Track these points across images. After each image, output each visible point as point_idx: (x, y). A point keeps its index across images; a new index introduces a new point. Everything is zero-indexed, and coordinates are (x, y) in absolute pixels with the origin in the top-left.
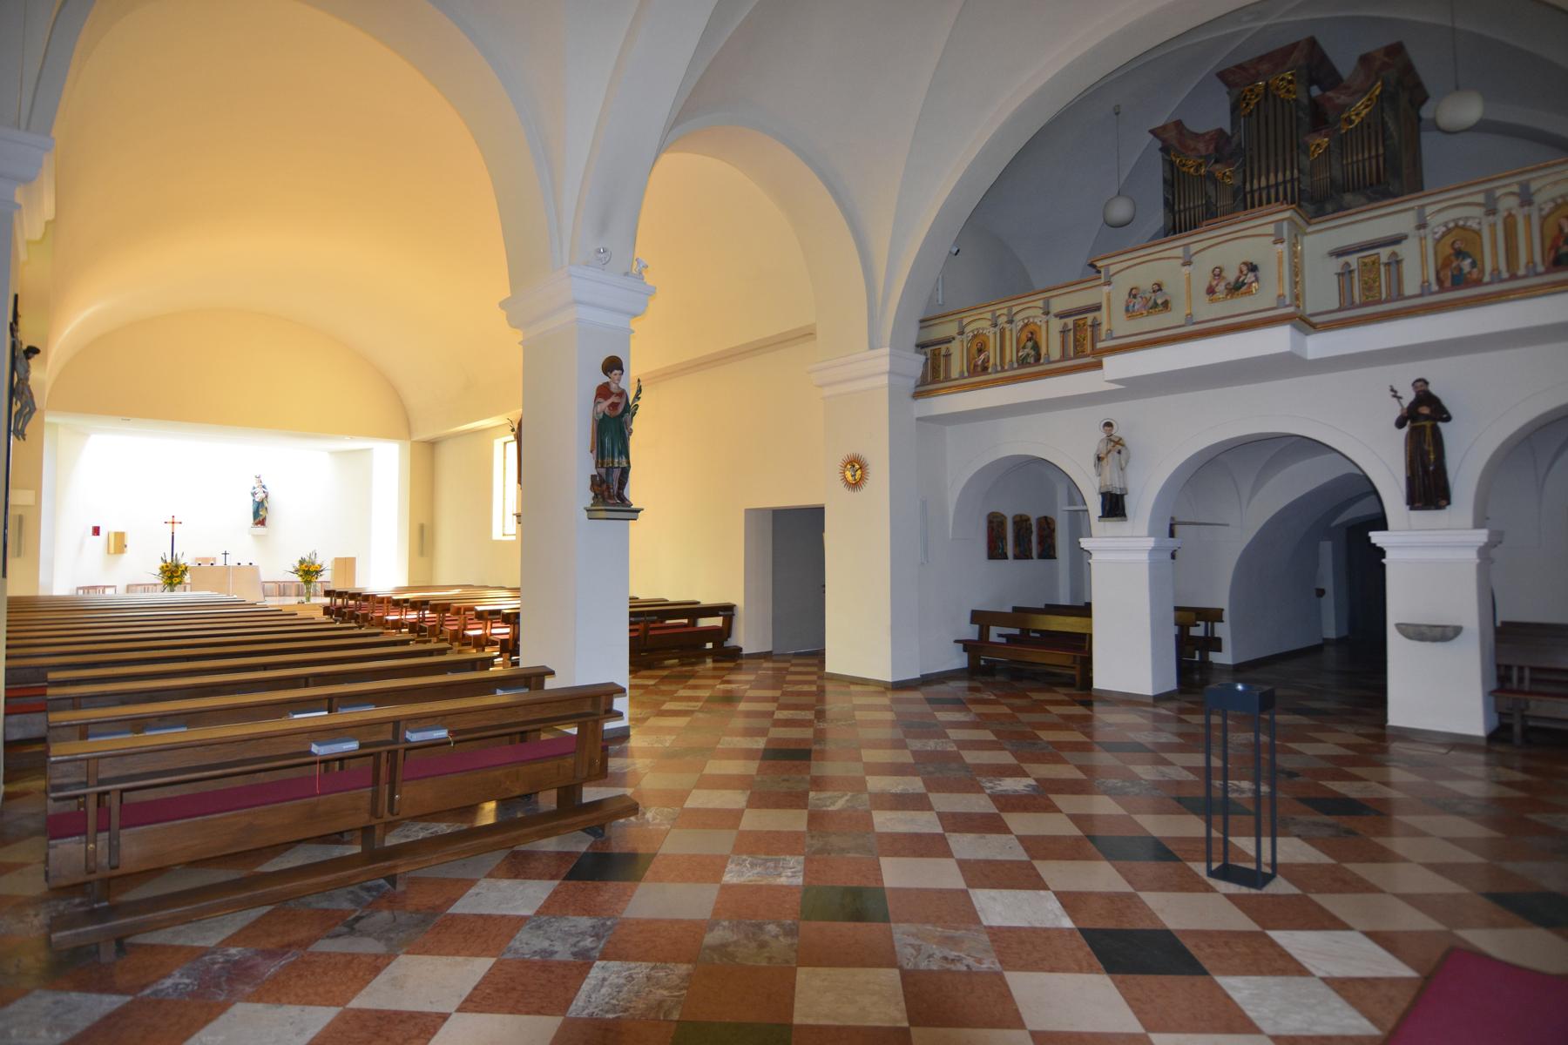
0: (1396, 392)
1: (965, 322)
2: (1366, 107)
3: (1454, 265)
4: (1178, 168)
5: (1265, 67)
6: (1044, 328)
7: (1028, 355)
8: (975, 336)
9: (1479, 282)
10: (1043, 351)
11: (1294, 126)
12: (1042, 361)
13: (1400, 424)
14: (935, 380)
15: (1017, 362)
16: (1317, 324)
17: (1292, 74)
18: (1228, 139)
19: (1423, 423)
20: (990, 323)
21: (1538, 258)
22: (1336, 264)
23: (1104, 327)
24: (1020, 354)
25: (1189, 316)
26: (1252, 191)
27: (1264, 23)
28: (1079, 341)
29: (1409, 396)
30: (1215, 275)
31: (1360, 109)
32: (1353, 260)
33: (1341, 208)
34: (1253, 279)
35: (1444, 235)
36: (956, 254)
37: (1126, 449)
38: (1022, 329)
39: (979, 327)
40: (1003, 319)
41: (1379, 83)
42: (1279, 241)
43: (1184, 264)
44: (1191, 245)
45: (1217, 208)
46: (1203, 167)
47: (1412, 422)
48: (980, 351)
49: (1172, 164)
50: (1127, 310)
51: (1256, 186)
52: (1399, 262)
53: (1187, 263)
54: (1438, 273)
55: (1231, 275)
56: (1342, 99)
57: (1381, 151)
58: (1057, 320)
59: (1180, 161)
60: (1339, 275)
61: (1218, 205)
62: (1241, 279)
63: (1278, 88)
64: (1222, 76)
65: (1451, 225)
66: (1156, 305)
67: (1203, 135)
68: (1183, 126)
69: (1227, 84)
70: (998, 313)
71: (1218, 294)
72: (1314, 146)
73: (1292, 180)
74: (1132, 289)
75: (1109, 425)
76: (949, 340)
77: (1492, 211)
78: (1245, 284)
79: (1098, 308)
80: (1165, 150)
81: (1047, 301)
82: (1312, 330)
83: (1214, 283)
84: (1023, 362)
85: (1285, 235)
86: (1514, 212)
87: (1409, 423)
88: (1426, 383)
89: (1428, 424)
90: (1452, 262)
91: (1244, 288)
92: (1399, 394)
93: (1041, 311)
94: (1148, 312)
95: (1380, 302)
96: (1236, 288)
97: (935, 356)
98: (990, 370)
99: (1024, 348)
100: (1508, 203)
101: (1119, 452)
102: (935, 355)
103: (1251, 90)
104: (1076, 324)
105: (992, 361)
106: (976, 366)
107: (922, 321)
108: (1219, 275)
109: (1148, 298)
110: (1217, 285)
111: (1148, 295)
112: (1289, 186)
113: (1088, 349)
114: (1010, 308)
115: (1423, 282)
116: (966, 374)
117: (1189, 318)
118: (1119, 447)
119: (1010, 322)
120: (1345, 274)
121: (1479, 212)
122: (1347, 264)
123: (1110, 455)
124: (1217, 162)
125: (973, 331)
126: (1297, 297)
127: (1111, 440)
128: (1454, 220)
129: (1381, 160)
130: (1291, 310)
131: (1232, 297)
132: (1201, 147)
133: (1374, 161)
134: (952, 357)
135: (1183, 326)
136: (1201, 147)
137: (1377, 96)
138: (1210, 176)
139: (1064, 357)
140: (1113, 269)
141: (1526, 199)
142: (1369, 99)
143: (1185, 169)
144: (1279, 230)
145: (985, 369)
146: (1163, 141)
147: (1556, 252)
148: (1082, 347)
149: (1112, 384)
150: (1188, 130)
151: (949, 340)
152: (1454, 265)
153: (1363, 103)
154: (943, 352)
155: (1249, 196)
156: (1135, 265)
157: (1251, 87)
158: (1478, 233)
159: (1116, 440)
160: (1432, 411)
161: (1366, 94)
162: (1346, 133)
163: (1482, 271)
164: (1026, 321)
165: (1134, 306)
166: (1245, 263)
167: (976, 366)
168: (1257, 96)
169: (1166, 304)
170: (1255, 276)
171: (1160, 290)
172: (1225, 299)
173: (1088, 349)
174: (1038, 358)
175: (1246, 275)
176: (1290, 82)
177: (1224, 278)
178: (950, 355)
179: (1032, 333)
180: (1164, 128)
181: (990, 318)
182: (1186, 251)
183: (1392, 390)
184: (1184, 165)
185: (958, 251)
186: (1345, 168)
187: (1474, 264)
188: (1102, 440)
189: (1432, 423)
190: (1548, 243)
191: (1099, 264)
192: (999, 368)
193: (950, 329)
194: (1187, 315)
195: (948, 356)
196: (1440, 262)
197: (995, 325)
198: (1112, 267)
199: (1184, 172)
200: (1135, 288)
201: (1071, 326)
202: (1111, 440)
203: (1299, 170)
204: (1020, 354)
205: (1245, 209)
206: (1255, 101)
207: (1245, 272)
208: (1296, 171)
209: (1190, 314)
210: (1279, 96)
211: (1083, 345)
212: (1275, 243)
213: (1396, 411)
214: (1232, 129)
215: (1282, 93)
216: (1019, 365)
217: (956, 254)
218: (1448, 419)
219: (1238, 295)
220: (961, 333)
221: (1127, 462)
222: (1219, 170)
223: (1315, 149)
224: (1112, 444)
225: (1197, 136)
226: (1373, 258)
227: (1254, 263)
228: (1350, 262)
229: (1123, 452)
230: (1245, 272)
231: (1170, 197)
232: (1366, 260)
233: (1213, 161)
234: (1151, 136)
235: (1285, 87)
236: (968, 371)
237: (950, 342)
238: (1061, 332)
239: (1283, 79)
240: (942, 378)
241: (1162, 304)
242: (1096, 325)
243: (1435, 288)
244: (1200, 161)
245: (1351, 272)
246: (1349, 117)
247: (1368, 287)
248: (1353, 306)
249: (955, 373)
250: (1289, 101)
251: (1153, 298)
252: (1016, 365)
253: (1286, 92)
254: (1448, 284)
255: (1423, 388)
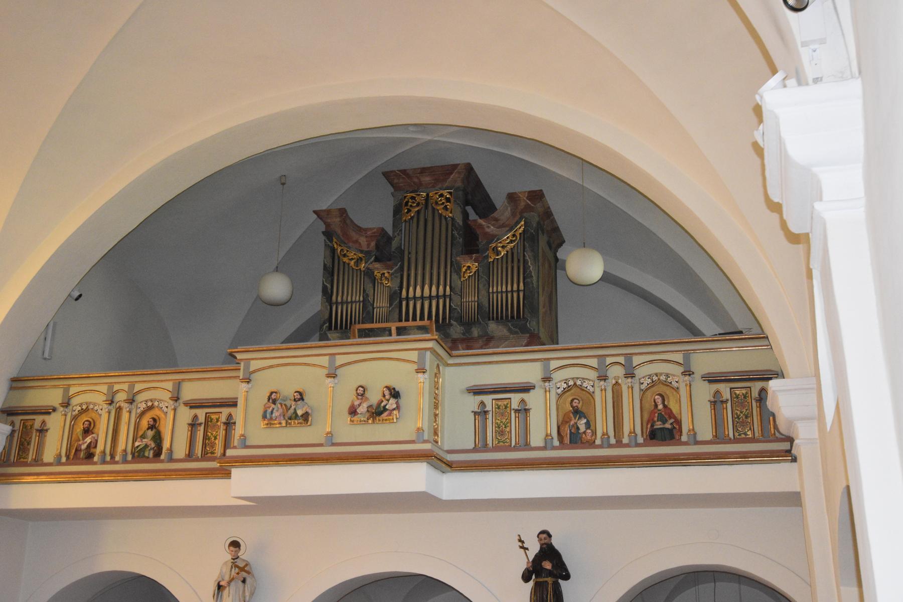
0: (523, 542)
1: (73, 390)
2: (511, 242)
3: (572, 423)
4: (339, 257)
5: (426, 179)
6: (171, 415)
7: (146, 446)
8: (83, 412)
9: (591, 444)
10: (166, 445)
11: (449, 243)
12: (162, 457)
13: (526, 577)
14: (21, 461)
15: (133, 454)
16: (452, 462)
17: (450, 193)
18: (389, 239)
19: (546, 579)
20: (105, 398)
21: (638, 430)
22: (473, 402)
23: (238, 430)
24: (137, 444)
25: (330, 435)
26: (407, 299)
27: (429, 138)
28: (209, 439)
29: (534, 548)
30: (358, 394)
31: (506, 242)
32: (488, 399)
33: (488, 340)
34: (395, 406)
35: (565, 391)
36: (77, 299)
37: (253, 576)
38: (143, 413)
39: (89, 400)
40: (121, 397)
41: (523, 223)
42: (421, 370)
43: (329, 376)
44: (337, 357)
45: (373, 308)
46: (363, 262)
47: (536, 577)
48: (87, 431)
49: (333, 250)
50: (264, 417)
51: (418, 294)
52: (527, 411)
53: (332, 375)
54: (559, 428)
55: (374, 397)
56: (491, 229)
57: (522, 287)
58: (187, 408)
59: (342, 250)
60: (475, 413)
61: (375, 306)
62: (383, 404)
63: (437, 203)
64: (387, 175)
65: (571, 383)
66: (295, 416)
67: (366, 230)
68: (347, 214)
69: (396, 187)
70: (116, 387)
71: (359, 415)
72: (465, 268)
73: (444, 296)
74: (272, 393)
75: (235, 544)
76: (47, 411)
77: (603, 378)
78: (387, 410)
79: (234, 404)
80: (328, 234)
81: (178, 386)
82: (449, 469)
83: (357, 403)
84: (139, 455)
85: (427, 367)
86: (620, 381)
87: (534, 577)
88: (550, 536)
89: (550, 580)
90: (571, 420)
91: (386, 414)
92: (525, 546)
93: (170, 395)
94: (287, 422)
95: (509, 448)
96: (377, 412)
97: (26, 430)
98: (96, 459)
99: (143, 437)
100: (616, 372)
101: (244, 581)
102: (25, 426)
103: (413, 198)
104: (208, 418)
105: (100, 447)
106: (78, 450)
107: (14, 380)
108: (362, 395)
109: (289, 406)
110: (359, 405)
111: (288, 403)
112: (441, 301)
113: (219, 450)
114: (132, 385)
115: (547, 435)
116: (64, 459)
117: (330, 439)
118: (244, 574)
119: (131, 401)
120: (481, 413)
121: (593, 375)
122: (482, 404)
123: (233, 584)
124: (377, 260)
125: (81, 405)
126: (436, 433)
127: (237, 566)
128: (573, 379)
129: (521, 294)
130: (427, 446)
131: (373, 422)
132: (363, 241)
133: (515, 295)
134: (49, 434)
135: (321, 445)
136: (363, 241)
137: (520, 234)
138: (369, 273)
139: (190, 456)
140: (254, 365)
141: (630, 375)
142: (514, 235)
143: (345, 260)
144: (422, 359)
145: (90, 456)
146: (328, 225)
147: (652, 426)
148: (213, 447)
149: (239, 500)
150: (352, 221)
151: (47, 411)
152: (572, 423)
153: (508, 238)
154: (37, 425)
155: (404, 303)
156: (278, 365)
157: (413, 195)
158: (592, 395)
159: (241, 565)
160: (553, 567)
161: (510, 230)
162: (493, 261)
163: (594, 433)
164: (150, 404)
165: (272, 412)
166: (387, 387)
167: (78, 450)
168: (418, 205)
169: (306, 417)
170: (397, 403)
171: (302, 399)
172: (366, 422)
173: (219, 450)
174: (158, 453)
175: (388, 400)
176: (448, 200)
177: (367, 399)
178: (47, 430)
179: (154, 420)
180: (328, 212)
181: (105, 392)
182: (332, 362)
183: (520, 540)
184: (345, 255)
185: (80, 296)
186: (491, 295)
187: (588, 426)
188: (226, 563)
189: (554, 580)
190: (646, 417)
191: (239, 356)
192: (108, 458)
193: (50, 396)
194: (328, 433)
195: (42, 431)
196: (561, 419)
197: (111, 402)
198: (252, 362)
199: (344, 263)
200: (276, 393)
201: (202, 419)
202: (237, 566)
203: (451, 287)
204: (137, 444)
205: (373, 323)
206: (417, 209)
207: (387, 397)
208: (448, 288)
209: (330, 433)
210: (438, 211)
211: (213, 445)
212: (418, 371)
213: (522, 563)
214: (394, 232)
215: (440, 208)
216: (133, 457)
217: (77, 299)
218: (567, 577)
219: (379, 420)
220: (66, 404)
221: (252, 594)
222: (379, 270)
223: (466, 270)
224: (237, 570)
225: (359, 230)
226: (505, 402)
227: (397, 390)
228: (486, 403)
229: (248, 581)
230: (387, 397)
231: (329, 286)
232: (500, 403)
233: (373, 259)
234: (315, 216)
235: (443, 203)
236: (68, 457)
237: (49, 413)
238: (189, 424)
239: (441, 195)
240: (30, 459)
241: (302, 416)
242: (229, 424)
243: (556, 443)
244: (360, 255)
245: (486, 412)
246: (496, 247)
247: (500, 431)
248: (485, 448)
249: (49, 455)
250: (446, 218)
251: (293, 407)
252: (130, 457)
253: (443, 208)
254: (567, 440)
255: (546, 541)
